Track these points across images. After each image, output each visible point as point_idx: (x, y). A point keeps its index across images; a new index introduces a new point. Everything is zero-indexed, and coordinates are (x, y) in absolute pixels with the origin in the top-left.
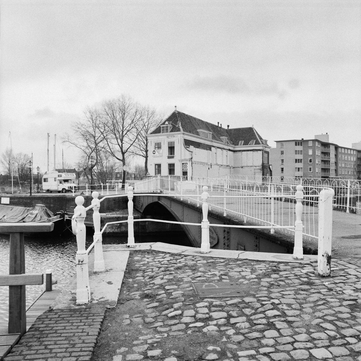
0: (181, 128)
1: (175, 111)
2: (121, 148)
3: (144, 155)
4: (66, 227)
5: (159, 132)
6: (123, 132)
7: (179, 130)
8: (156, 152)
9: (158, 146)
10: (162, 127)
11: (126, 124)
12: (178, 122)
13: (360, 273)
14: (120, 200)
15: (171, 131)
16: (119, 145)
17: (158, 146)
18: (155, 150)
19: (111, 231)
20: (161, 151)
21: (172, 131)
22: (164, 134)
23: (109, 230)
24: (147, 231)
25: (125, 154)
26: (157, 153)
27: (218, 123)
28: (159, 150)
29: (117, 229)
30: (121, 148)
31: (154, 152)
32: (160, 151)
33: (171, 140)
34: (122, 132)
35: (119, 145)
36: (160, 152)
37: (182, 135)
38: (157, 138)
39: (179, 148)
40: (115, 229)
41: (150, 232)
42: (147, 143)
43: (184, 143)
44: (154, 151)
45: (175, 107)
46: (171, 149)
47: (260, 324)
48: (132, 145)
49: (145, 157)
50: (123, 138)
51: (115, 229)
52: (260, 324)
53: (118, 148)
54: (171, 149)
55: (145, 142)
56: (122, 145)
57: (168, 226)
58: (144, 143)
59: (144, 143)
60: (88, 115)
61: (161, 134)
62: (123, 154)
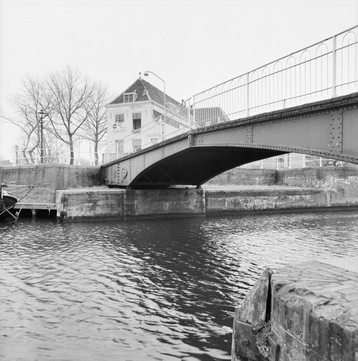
0: (148, 96)
1: (140, 78)
2: (69, 131)
3: (94, 139)
4: (3, 208)
5: (121, 101)
6: (70, 110)
7: (146, 98)
8: (118, 126)
9: (120, 119)
10: (125, 95)
11: (73, 103)
12: (144, 90)
13: (1, 288)
14: (85, 174)
15: (136, 100)
16: (65, 124)
17: (120, 119)
18: (116, 124)
19: (80, 215)
20: (124, 124)
21: (137, 100)
22: (127, 103)
23: (77, 213)
24: (137, 214)
25: (73, 136)
26: (118, 128)
27: (183, 101)
28: (121, 123)
29: (90, 210)
30: (69, 131)
31: (115, 126)
32: (123, 124)
33: (137, 110)
34: (68, 109)
35: (65, 124)
36: (123, 126)
37: (150, 105)
38: (116, 109)
39: (146, 119)
40: (87, 210)
41: (140, 216)
42: (97, 124)
43: (153, 115)
44: (115, 125)
45: (140, 73)
46: (137, 123)
47: (32, 301)
48: (79, 127)
49: (95, 141)
50: (70, 117)
51: (87, 210)
52: (32, 301)
53: (65, 129)
54: (137, 123)
55: (95, 123)
56: (69, 124)
57: (166, 205)
58: (94, 125)
59: (94, 125)
60: (29, 86)
61: (124, 103)
62: (70, 135)
